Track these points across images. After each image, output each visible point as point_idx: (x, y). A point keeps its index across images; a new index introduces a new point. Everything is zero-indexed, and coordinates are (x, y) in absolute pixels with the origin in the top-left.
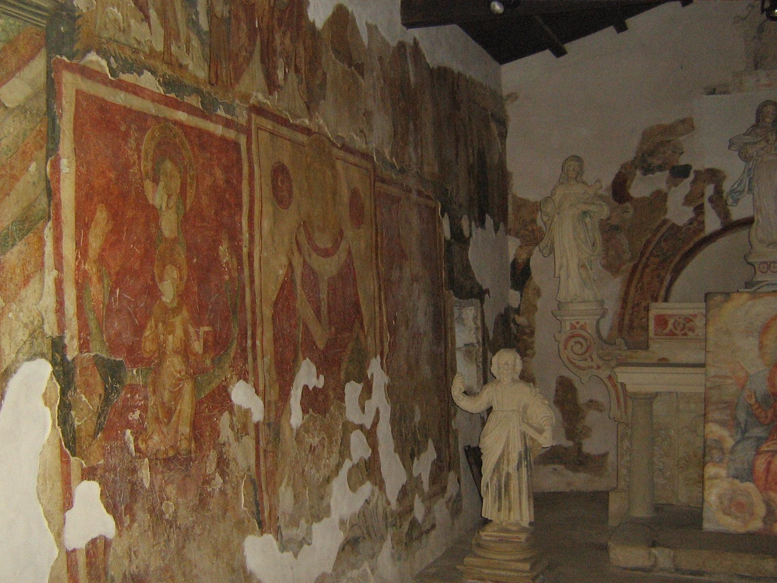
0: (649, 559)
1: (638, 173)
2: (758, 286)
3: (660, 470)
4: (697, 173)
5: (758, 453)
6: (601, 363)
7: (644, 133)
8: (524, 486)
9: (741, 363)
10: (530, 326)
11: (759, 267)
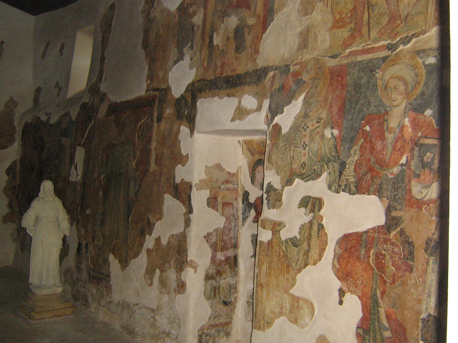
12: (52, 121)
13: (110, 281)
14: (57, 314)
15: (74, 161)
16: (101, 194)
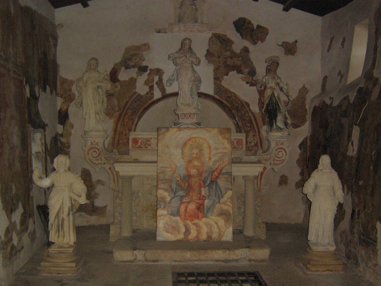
0: (133, 256)
1: (123, 68)
2: (181, 124)
3: (135, 213)
4: (151, 70)
5: (181, 203)
6: (106, 161)
7: (126, 49)
8: (71, 224)
9: (174, 161)
10: (68, 143)
11: (181, 115)
12: (335, 104)
13: (376, 246)
14: (329, 268)
15: (351, 139)
16: (371, 168)
